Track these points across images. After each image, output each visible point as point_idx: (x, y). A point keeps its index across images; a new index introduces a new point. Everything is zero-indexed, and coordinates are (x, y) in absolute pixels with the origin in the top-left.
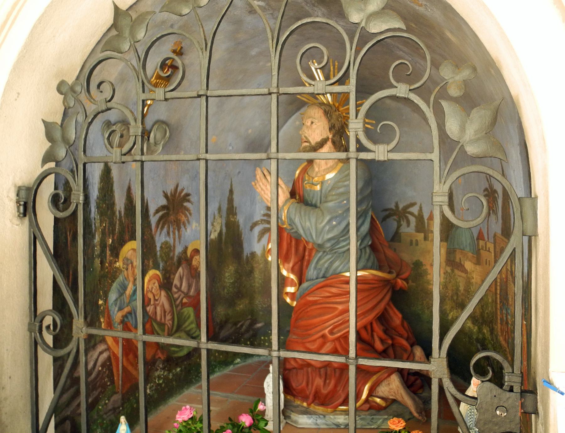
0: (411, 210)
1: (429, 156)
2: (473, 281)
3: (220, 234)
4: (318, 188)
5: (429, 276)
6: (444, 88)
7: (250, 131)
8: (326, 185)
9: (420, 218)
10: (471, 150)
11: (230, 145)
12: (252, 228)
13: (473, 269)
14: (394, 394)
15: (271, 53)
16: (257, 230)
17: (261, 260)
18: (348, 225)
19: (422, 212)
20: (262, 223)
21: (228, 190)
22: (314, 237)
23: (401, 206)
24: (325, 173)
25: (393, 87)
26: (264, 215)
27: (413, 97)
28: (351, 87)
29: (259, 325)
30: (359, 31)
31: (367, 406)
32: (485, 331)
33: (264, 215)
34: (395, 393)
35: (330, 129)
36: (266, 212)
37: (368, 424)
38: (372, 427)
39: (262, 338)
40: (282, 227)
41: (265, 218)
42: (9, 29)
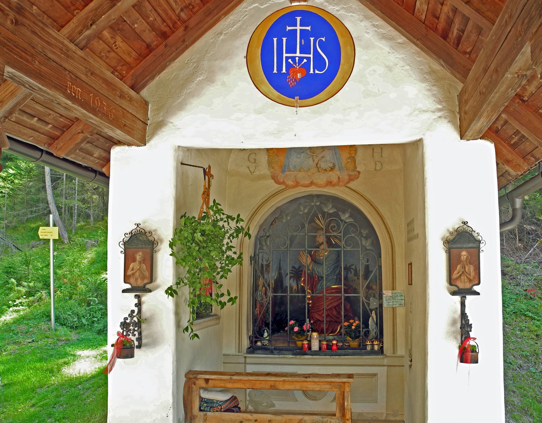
0: (352, 267)
1: (359, 249)
3: (277, 277)
6: (362, 235)
9: (356, 270)
10: (368, 248)
23: (348, 266)
25: (351, 234)
31: (339, 334)
42: (253, 219)
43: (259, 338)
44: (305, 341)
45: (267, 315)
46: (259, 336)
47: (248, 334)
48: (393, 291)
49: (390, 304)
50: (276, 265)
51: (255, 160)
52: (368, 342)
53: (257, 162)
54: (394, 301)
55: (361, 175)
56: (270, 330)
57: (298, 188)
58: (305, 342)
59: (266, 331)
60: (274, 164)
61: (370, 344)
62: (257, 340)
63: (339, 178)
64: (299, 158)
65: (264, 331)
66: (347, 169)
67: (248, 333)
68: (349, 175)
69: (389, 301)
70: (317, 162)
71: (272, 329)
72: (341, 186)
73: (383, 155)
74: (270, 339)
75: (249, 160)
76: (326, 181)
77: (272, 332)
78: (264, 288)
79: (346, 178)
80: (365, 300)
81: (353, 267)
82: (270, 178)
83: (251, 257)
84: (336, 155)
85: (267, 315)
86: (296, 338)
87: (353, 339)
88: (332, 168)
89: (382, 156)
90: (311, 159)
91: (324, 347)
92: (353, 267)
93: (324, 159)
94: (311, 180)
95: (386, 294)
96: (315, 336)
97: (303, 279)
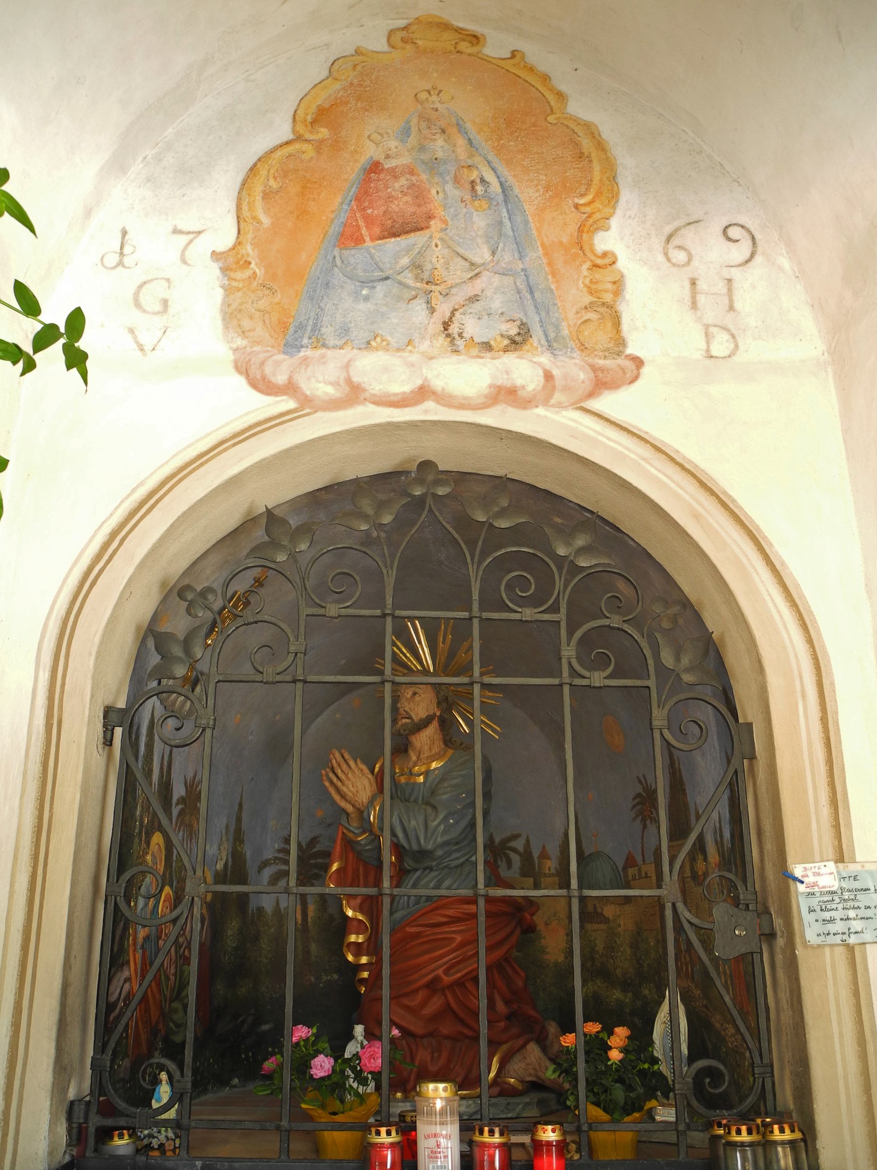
0: (513, 844)
1: (646, 683)
2: (620, 930)
3: (226, 865)
4: (421, 779)
5: (543, 941)
7: (278, 718)
8: (430, 778)
9: (527, 856)
11: (251, 734)
12: (261, 869)
13: (618, 913)
14: (532, 1072)
15: (472, 578)
16: (267, 873)
17: (272, 921)
18: (474, 817)
19: (529, 847)
20: (275, 862)
21: (238, 802)
22: (422, 841)
23: (497, 840)
24: (429, 761)
26: (279, 851)
27: (626, 627)
28: (561, 616)
29: (265, 1027)
30: (566, 564)
31: (496, 1090)
32: (647, 992)
33: (280, 851)
34: (535, 1070)
35: (439, 703)
36: (283, 846)
37: (502, 1111)
38: (510, 1115)
39: (270, 1049)
40: (355, 839)
41: (281, 855)
43: (122, 1114)
44: (383, 1130)
45: (176, 1011)
46: (121, 1105)
47: (64, 1090)
48: (841, 865)
49: (833, 928)
50: (225, 821)
51: (165, 303)
52: (744, 1128)
53: (171, 311)
54: (852, 914)
55: (645, 371)
56: (188, 1072)
57: (360, 409)
58: (385, 1138)
59: (164, 1076)
60: (251, 318)
61: (751, 1144)
62: (109, 1122)
63: (548, 376)
64: (367, 299)
65: (156, 1082)
66: (583, 347)
67: (59, 1086)
68: (594, 369)
69: (827, 915)
70: (448, 315)
71: (195, 1072)
72: (560, 406)
73: (738, 305)
74: (185, 1121)
75: (137, 304)
76: (490, 386)
77: (195, 1084)
78: (167, 889)
79: (583, 376)
80: (687, 915)
81: (519, 844)
82: (230, 367)
83: (108, 711)
84: (532, 292)
85: (176, 1011)
86: (323, 1117)
87: (616, 1116)
88: (517, 339)
89: (731, 308)
90: (419, 306)
91: (492, 1162)
92: (519, 844)
93: (477, 307)
94: (419, 382)
95: (805, 880)
96: (439, 1104)
97: (335, 867)
